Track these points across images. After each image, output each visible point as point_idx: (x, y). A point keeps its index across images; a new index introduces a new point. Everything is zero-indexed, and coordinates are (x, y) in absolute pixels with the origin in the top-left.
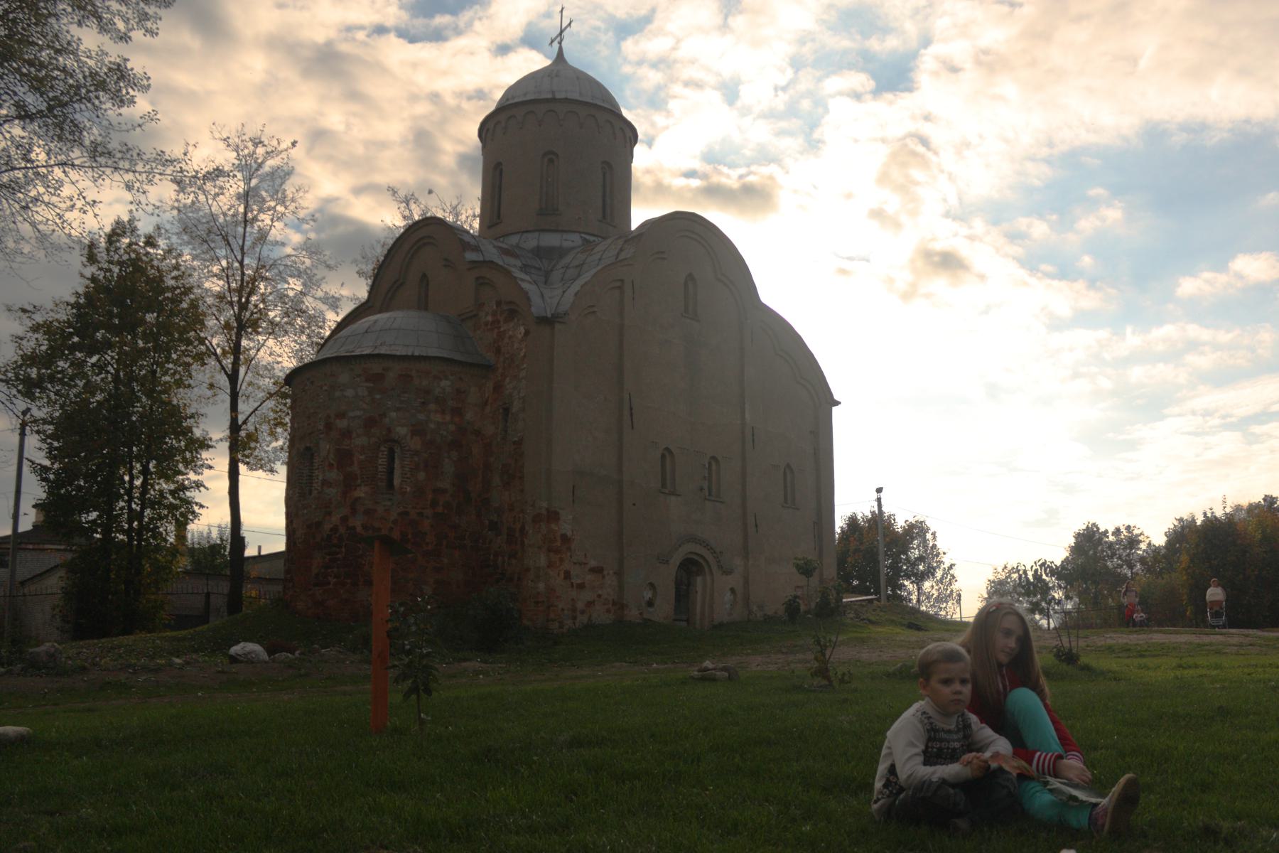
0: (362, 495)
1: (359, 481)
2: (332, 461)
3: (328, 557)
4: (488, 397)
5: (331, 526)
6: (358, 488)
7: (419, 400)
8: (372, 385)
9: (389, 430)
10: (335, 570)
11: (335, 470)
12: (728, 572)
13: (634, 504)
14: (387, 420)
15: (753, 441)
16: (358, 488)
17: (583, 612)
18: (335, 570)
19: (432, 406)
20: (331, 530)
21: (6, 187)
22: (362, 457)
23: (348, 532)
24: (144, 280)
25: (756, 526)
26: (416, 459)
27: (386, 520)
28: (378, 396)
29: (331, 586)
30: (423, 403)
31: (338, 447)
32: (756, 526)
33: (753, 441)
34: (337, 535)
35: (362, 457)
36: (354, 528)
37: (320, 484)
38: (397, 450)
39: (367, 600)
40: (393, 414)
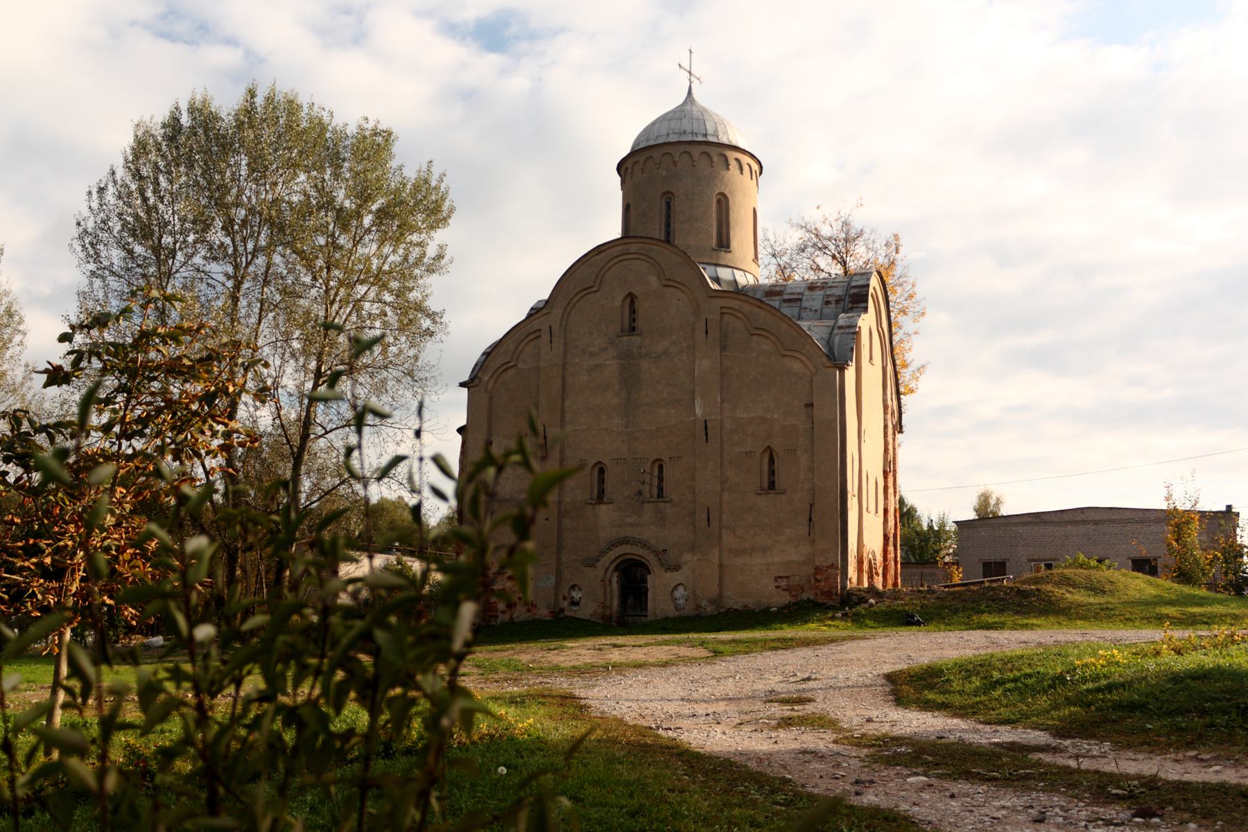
12: (677, 568)
13: (547, 519)
15: (706, 434)
17: (503, 612)
25: (709, 519)
32: (709, 519)
33: (706, 434)
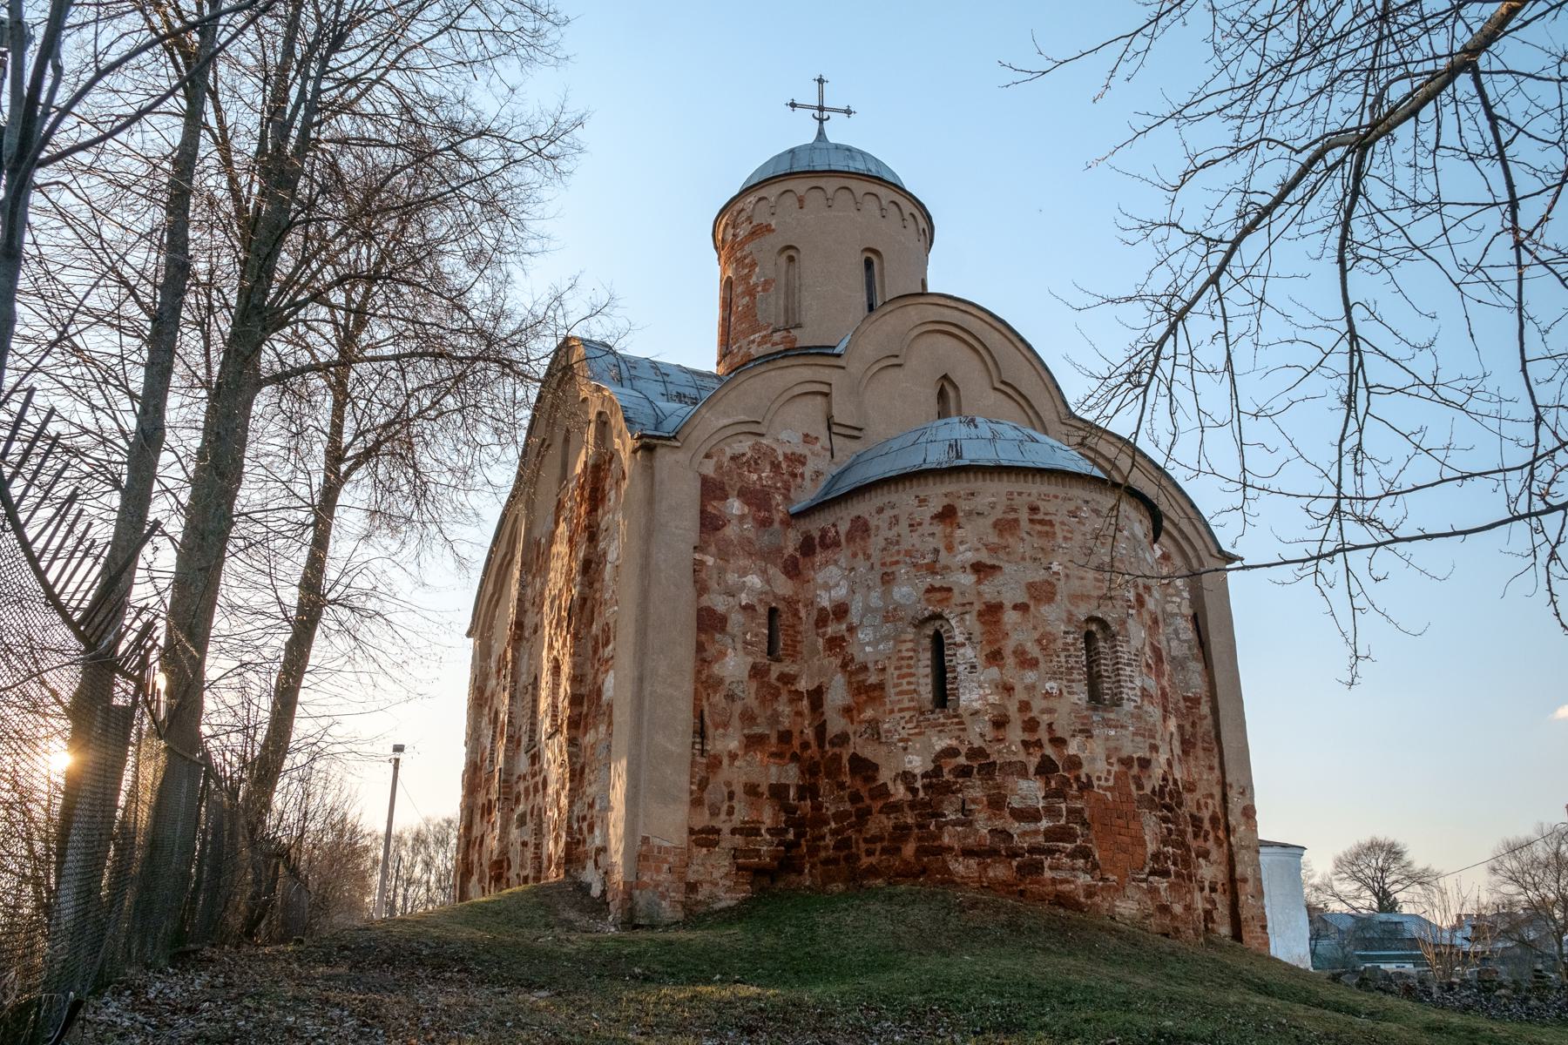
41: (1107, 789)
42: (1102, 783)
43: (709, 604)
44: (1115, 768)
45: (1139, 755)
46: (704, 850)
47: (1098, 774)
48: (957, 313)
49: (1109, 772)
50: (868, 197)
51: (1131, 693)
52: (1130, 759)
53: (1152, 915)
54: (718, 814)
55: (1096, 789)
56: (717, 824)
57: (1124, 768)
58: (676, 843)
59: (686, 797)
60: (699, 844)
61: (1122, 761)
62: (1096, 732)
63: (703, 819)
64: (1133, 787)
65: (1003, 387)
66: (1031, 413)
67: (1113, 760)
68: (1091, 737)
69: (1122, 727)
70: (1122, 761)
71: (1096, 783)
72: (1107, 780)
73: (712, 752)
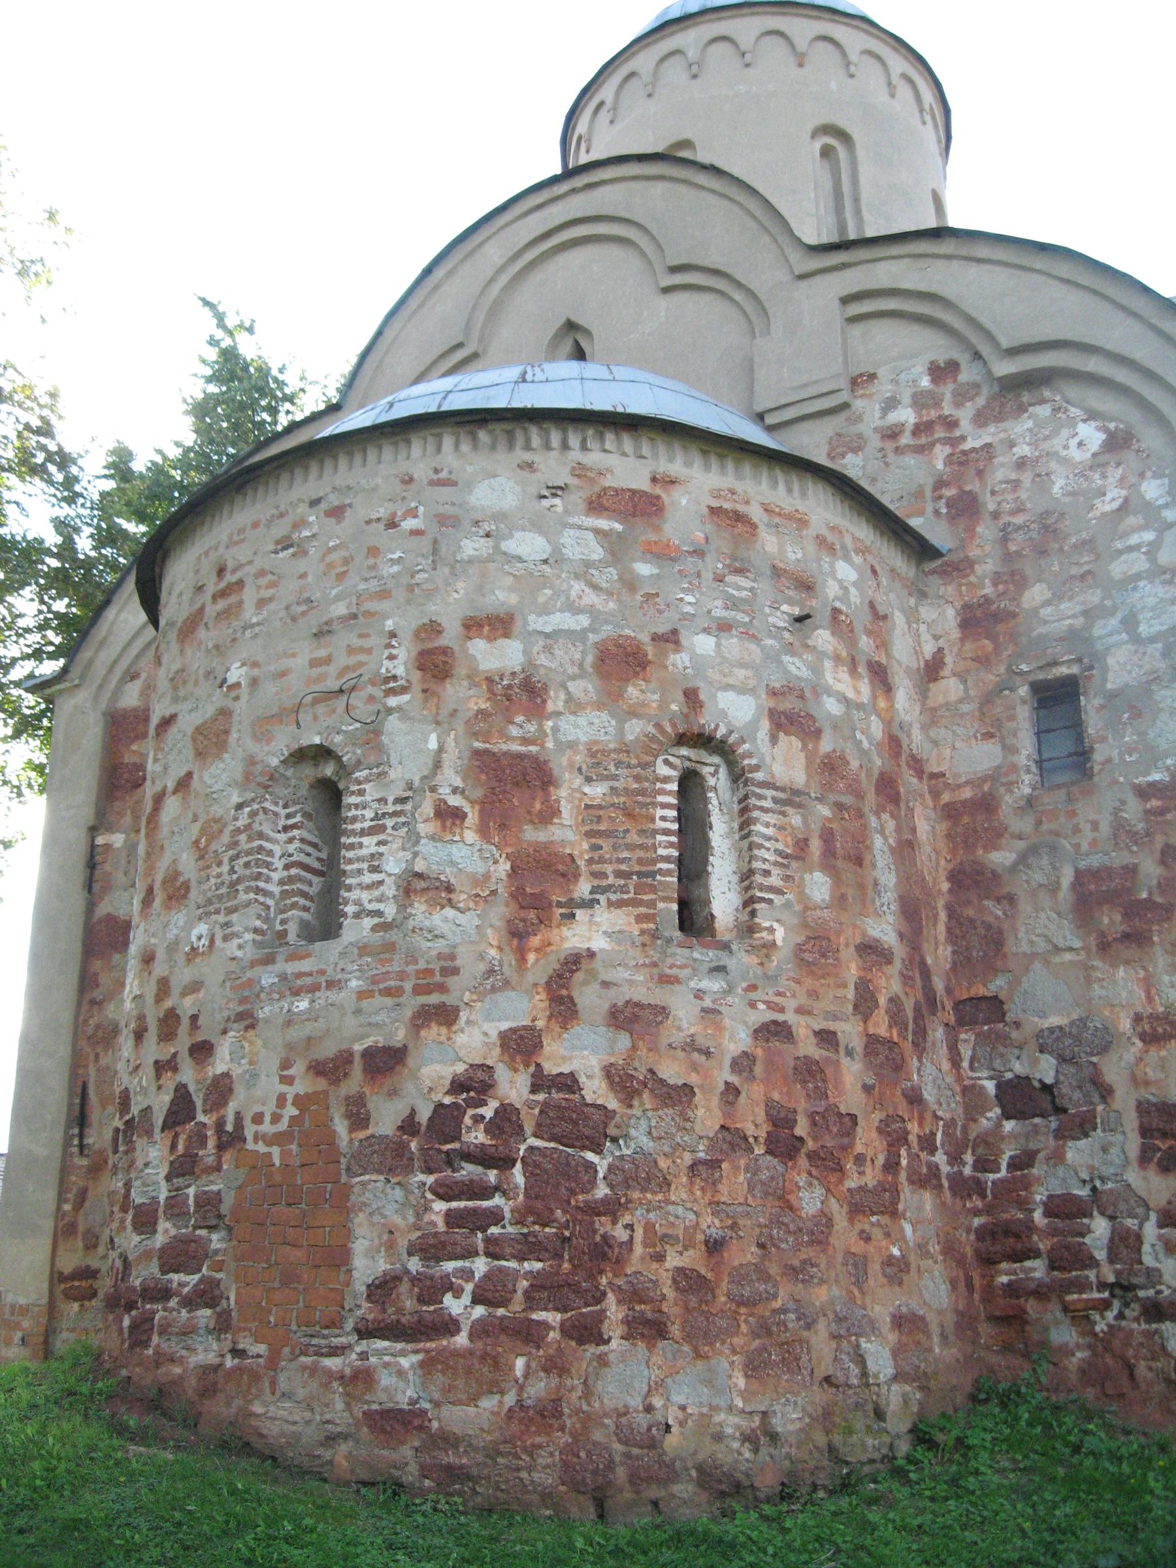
0: (599, 943)
1: (583, 888)
2: (455, 801)
3: (440, 1206)
4: (441, 749)
5: (460, 1068)
6: (580, 914)
7: (785, 608)
8: (618, 527)
9: (692, 697)
10: (481, 1265)
11: (470, 836)
14: (679, 660)
16: (580, 914)
18: (481, 1265)
19: (823, 638)
20: (458, 1086)
21: (820, 1158)
22: (597, 791)
23: (541, 1097)
24: (34, 456)
26: (796, 820)
27: (707, 1053)
28: (644, 569)
29: (462, 1340)
30: (800, 619)
31: (478, 745)
34: (488, 1112)
35: (597, 791)
36: (569, 1083)
37: (389, 889)
38: (717, 779)
39: (649, 1409)
40: (704, 644)
41: (270, 1140)
42: (267, 1127)
43: (110, 910)
44: (301, 1087)
45: (369, 1042)
46: (76, 1306)
47: (258, 1108)
48: (537, 216)
49: (281, 1100)
50: (768, 40)
51: (365, 896)
52: (345, 1059)
53: (345, 1437)
54: (95, 1246)
55: (250, 1145)
56: (94, 1263)
57: (321, 1084)
58: (33, 1297)
59: (48, 1224)
60: (70, 1296)
61: (318, 1069)
62: (264, 1012)
63: (69, 1262)
64: (341, 1127)
65: (678, 279)
66: (738, 296)
67: (298, 1069)
68: (252, 1026)
69: (330, 985)
70: (318, 1069)
71: (250, 1130)
72: (276, 1118)
73: (96, 1147)
